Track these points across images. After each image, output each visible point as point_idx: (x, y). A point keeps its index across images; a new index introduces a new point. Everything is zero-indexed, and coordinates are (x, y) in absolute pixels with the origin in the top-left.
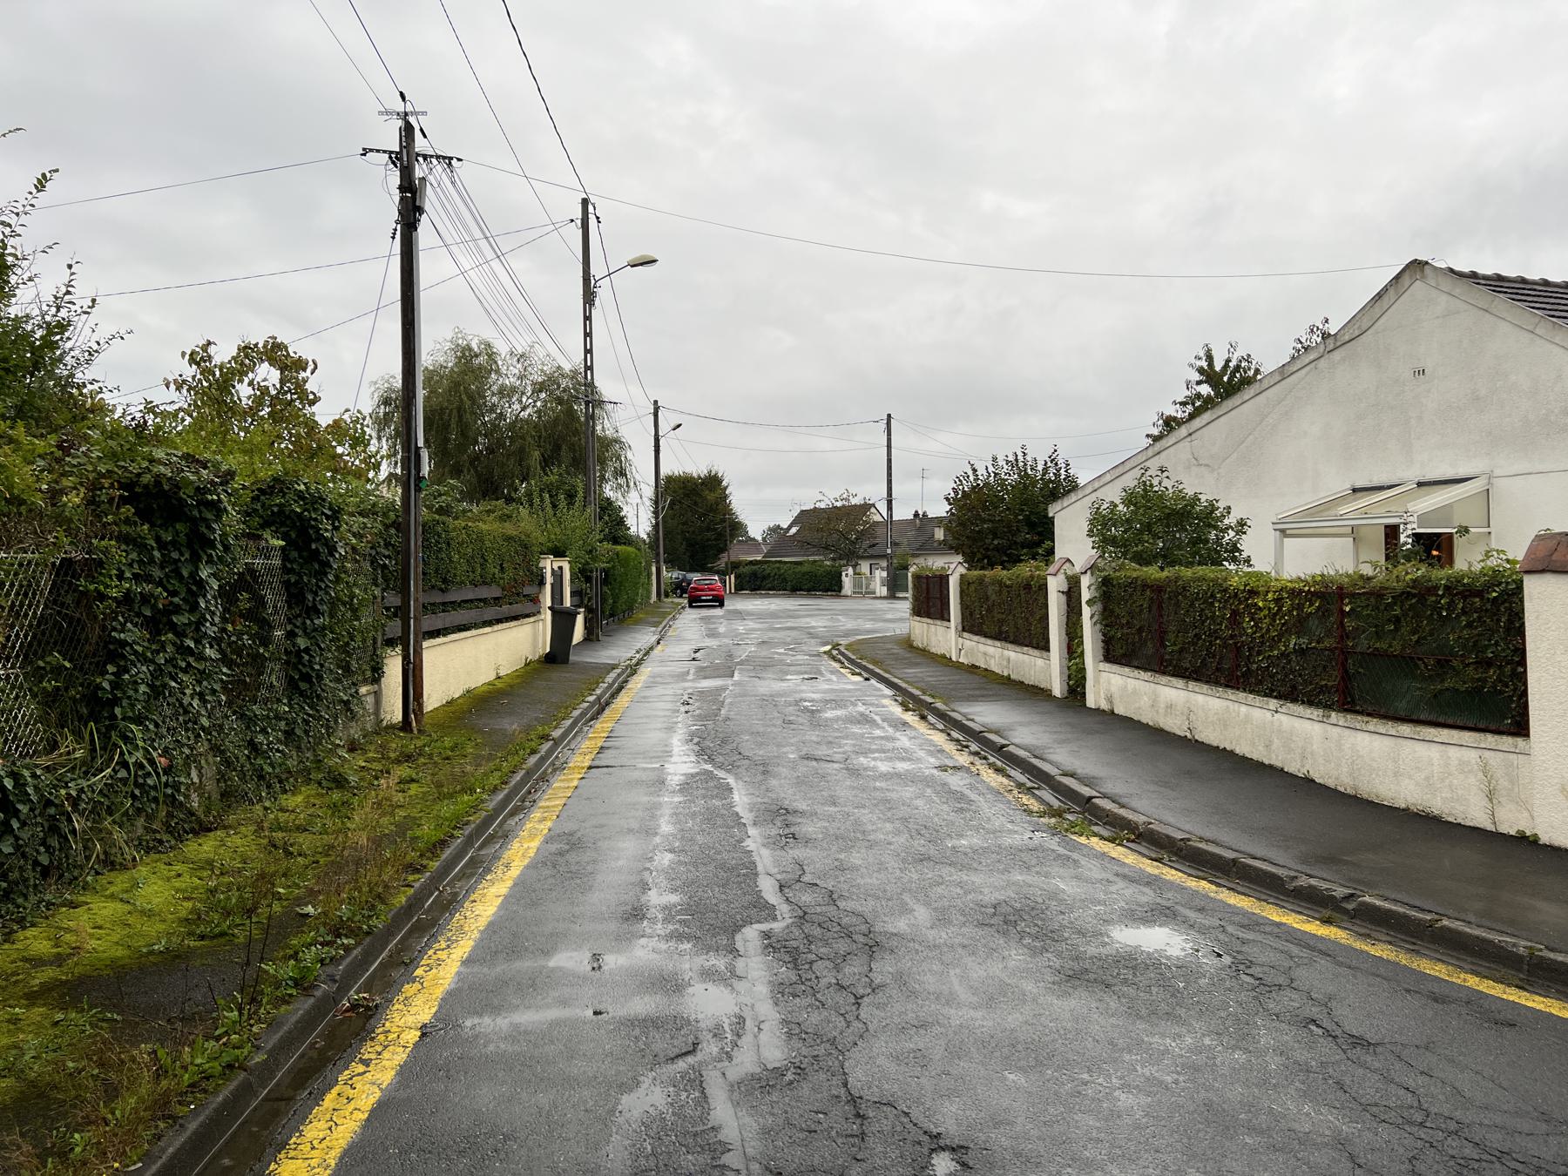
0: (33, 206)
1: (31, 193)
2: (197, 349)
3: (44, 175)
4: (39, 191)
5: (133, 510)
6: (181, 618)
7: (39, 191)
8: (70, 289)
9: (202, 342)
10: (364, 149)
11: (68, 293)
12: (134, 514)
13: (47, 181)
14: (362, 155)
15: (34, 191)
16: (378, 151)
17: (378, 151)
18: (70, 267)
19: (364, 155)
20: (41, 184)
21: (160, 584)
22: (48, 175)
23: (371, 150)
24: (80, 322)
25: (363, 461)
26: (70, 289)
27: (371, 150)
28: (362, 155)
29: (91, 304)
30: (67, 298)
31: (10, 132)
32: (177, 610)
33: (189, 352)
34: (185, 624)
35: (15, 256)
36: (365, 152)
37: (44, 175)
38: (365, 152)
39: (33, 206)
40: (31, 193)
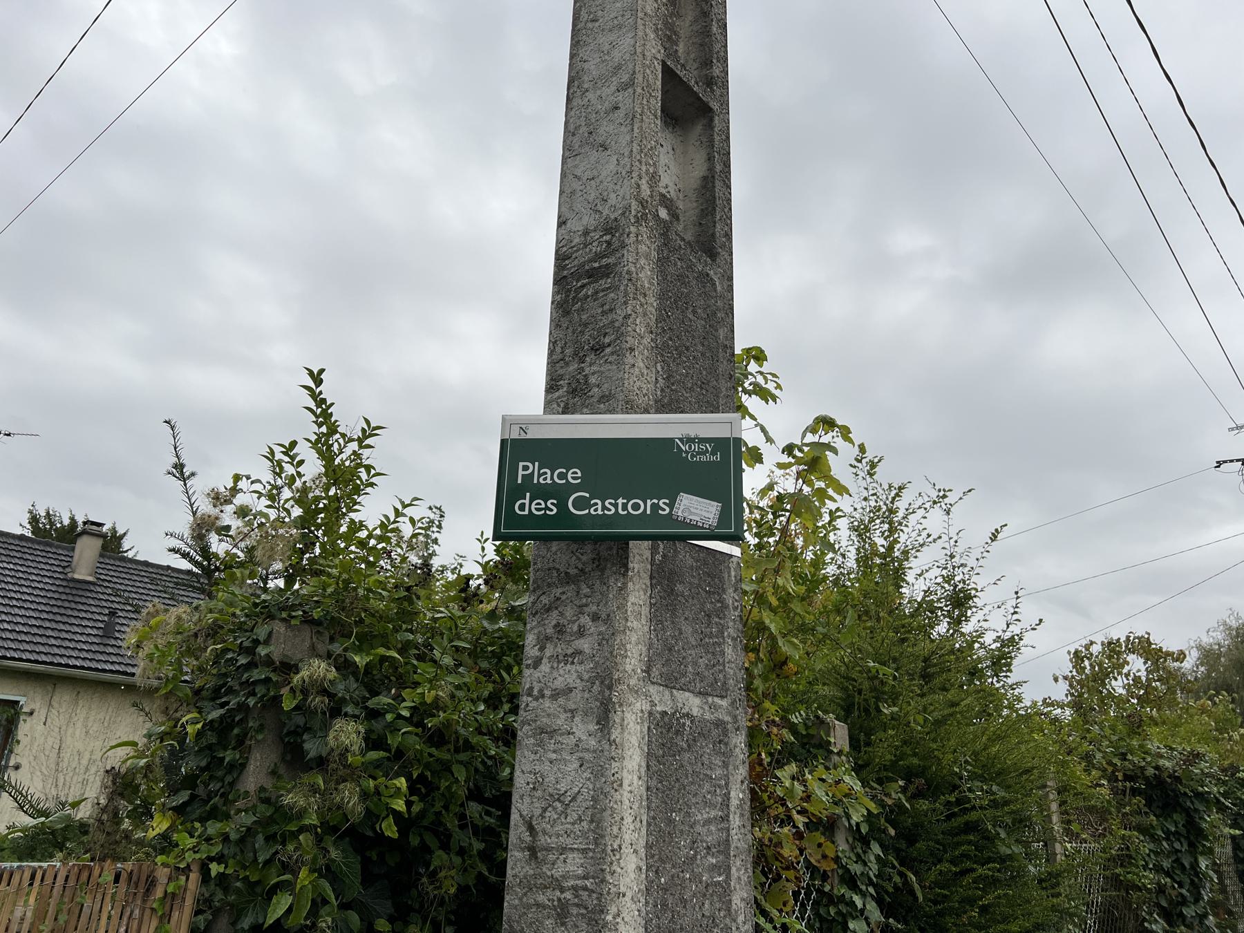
0: (988, 551)
1: (987, 543)
2: (1080, 649)
3: (996, 530)
4: (992, 541)
5: (1144, 802)
6: (1188, 910)
7: (992, 541)
8: (1016, 610)
9: (1084, 642)
10: (1217, 462)
11: (1015, 613)
12: (1145, 805)
13: (998, 533)
14: (1216, 467)
15: (990, 541)
16: (1232, 461)
17: (1232, 461)
18: (1017, 593)
19: (1218, 467)
20: (994, 537)
21: (1168, 874)
22: (999, 530)
23: (1225, 462)
24: (1028, 638)
25: (1140, 746)
26: (1016, 610)
27: (1225, 462)
28: (1216, 467)
29: (1038, 622)
30: (1015, 617)
31: (961, 499)
32: (1184, 902)
33: (1073, 651)
34: (1192, 917)
35: (976, 590)
36: (1219, 464)
37: (996, 530)
38: (1219, 464)
39: (988, 551)
40: (987, 543)
